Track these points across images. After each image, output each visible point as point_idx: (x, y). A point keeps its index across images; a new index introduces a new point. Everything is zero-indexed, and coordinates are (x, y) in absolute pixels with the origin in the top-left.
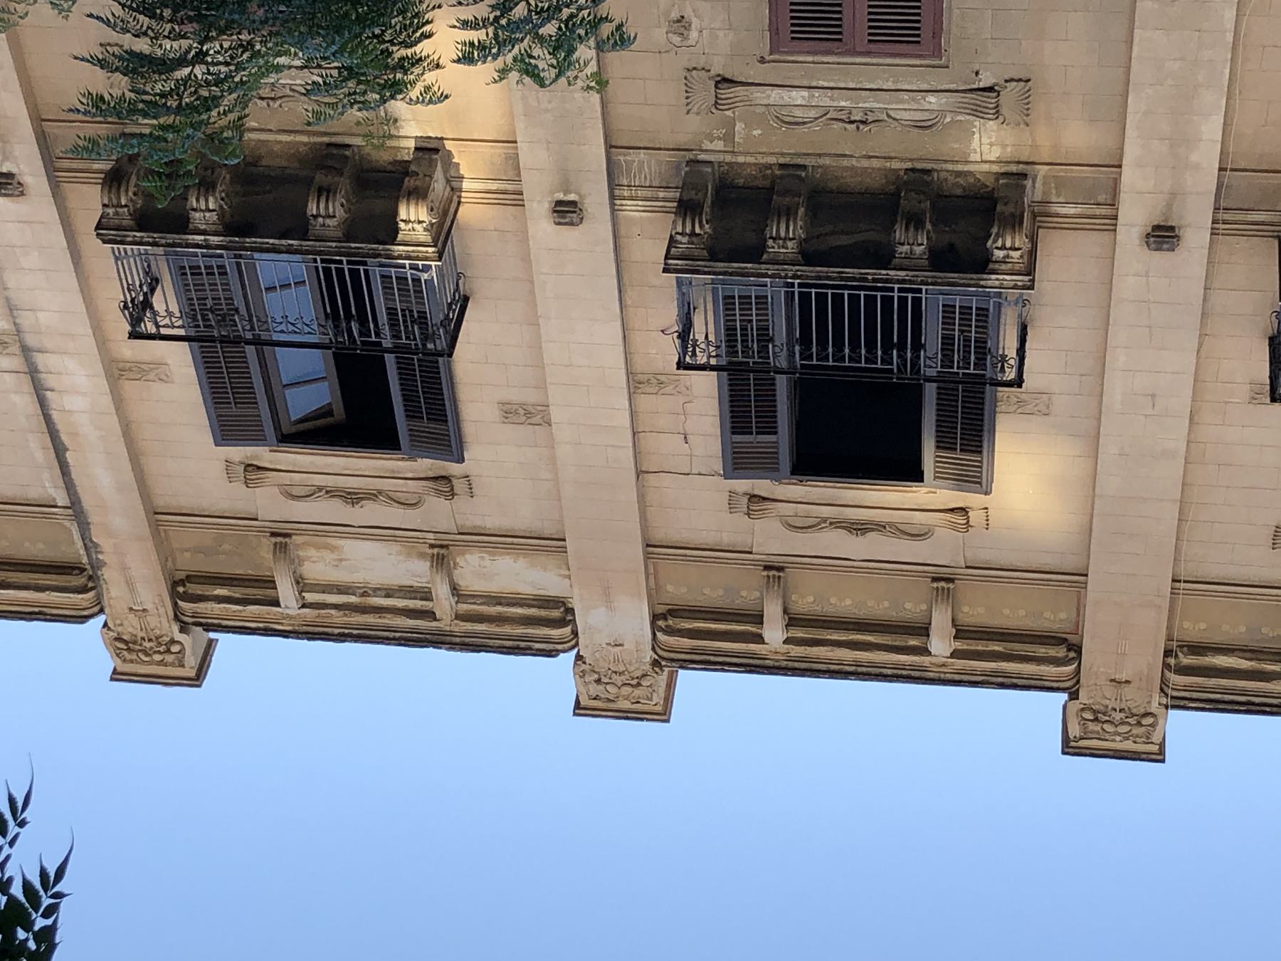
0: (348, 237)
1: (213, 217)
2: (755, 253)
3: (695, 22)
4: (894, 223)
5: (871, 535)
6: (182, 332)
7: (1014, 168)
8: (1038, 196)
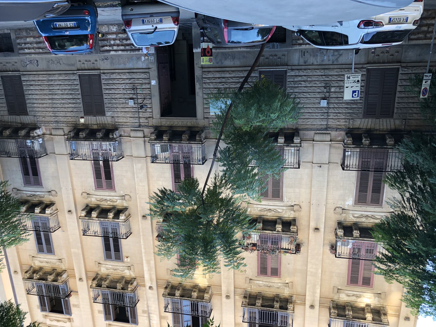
0: (197, 298)
1: (179, 294)
2: (254, 305)
3: (247, 271)
4: (274, 302)
5: (61, 322)
6: (101, 302)
7: (291, 295)
8: (294, 300)
